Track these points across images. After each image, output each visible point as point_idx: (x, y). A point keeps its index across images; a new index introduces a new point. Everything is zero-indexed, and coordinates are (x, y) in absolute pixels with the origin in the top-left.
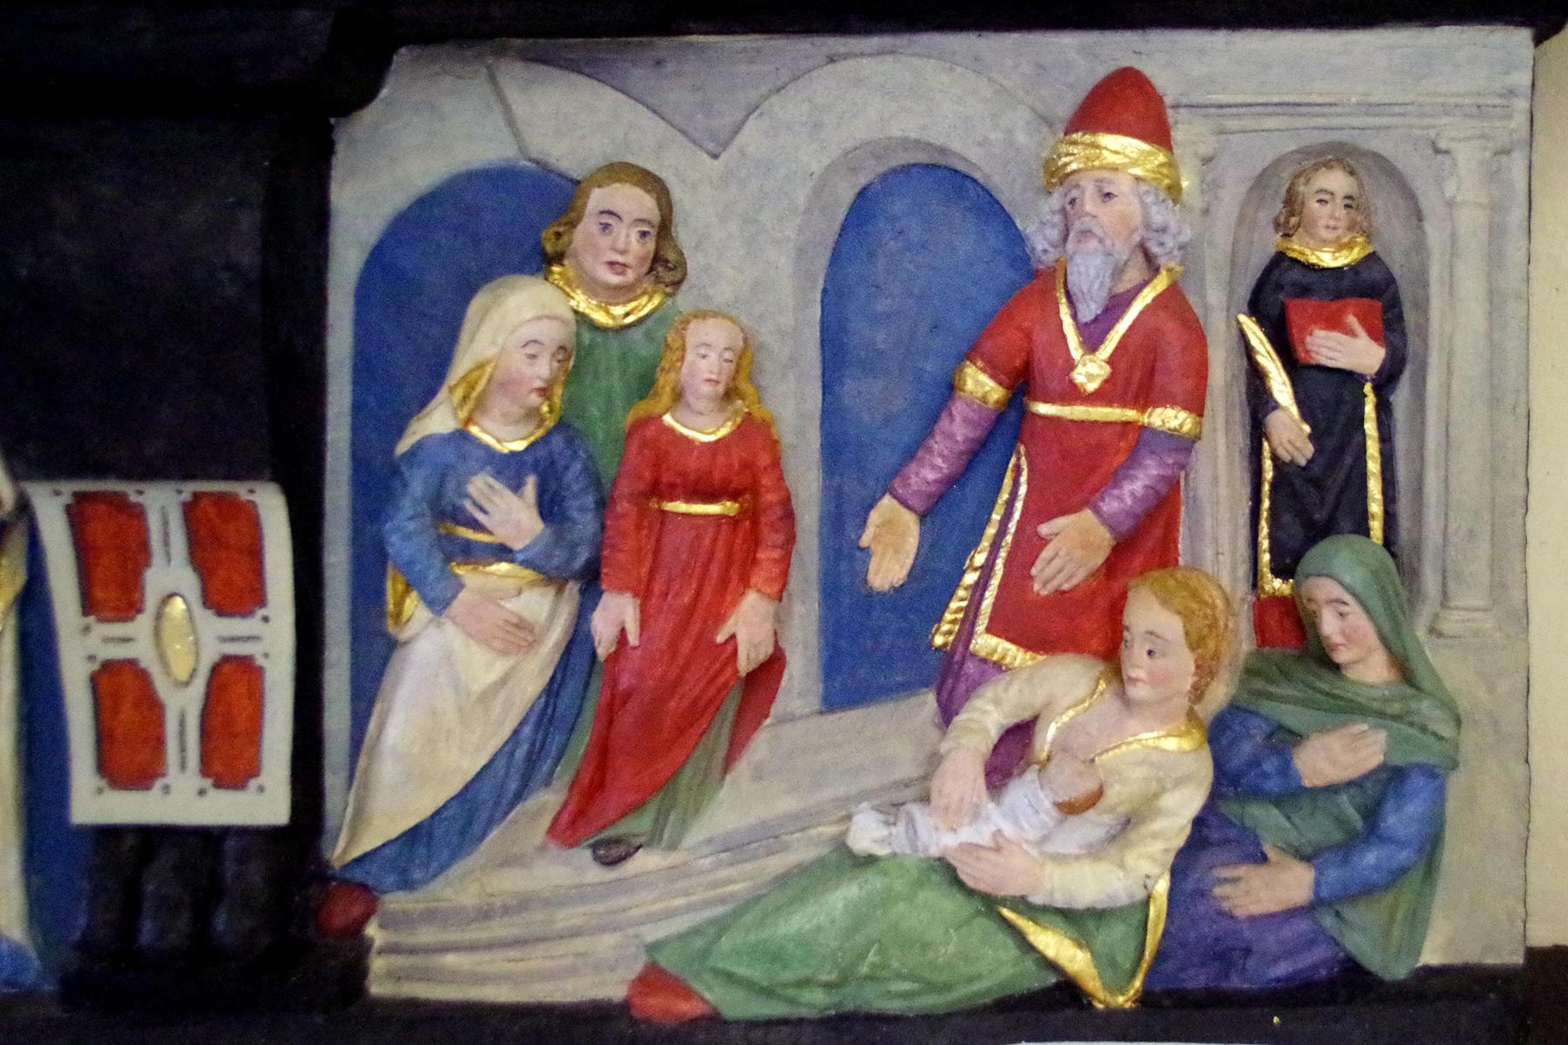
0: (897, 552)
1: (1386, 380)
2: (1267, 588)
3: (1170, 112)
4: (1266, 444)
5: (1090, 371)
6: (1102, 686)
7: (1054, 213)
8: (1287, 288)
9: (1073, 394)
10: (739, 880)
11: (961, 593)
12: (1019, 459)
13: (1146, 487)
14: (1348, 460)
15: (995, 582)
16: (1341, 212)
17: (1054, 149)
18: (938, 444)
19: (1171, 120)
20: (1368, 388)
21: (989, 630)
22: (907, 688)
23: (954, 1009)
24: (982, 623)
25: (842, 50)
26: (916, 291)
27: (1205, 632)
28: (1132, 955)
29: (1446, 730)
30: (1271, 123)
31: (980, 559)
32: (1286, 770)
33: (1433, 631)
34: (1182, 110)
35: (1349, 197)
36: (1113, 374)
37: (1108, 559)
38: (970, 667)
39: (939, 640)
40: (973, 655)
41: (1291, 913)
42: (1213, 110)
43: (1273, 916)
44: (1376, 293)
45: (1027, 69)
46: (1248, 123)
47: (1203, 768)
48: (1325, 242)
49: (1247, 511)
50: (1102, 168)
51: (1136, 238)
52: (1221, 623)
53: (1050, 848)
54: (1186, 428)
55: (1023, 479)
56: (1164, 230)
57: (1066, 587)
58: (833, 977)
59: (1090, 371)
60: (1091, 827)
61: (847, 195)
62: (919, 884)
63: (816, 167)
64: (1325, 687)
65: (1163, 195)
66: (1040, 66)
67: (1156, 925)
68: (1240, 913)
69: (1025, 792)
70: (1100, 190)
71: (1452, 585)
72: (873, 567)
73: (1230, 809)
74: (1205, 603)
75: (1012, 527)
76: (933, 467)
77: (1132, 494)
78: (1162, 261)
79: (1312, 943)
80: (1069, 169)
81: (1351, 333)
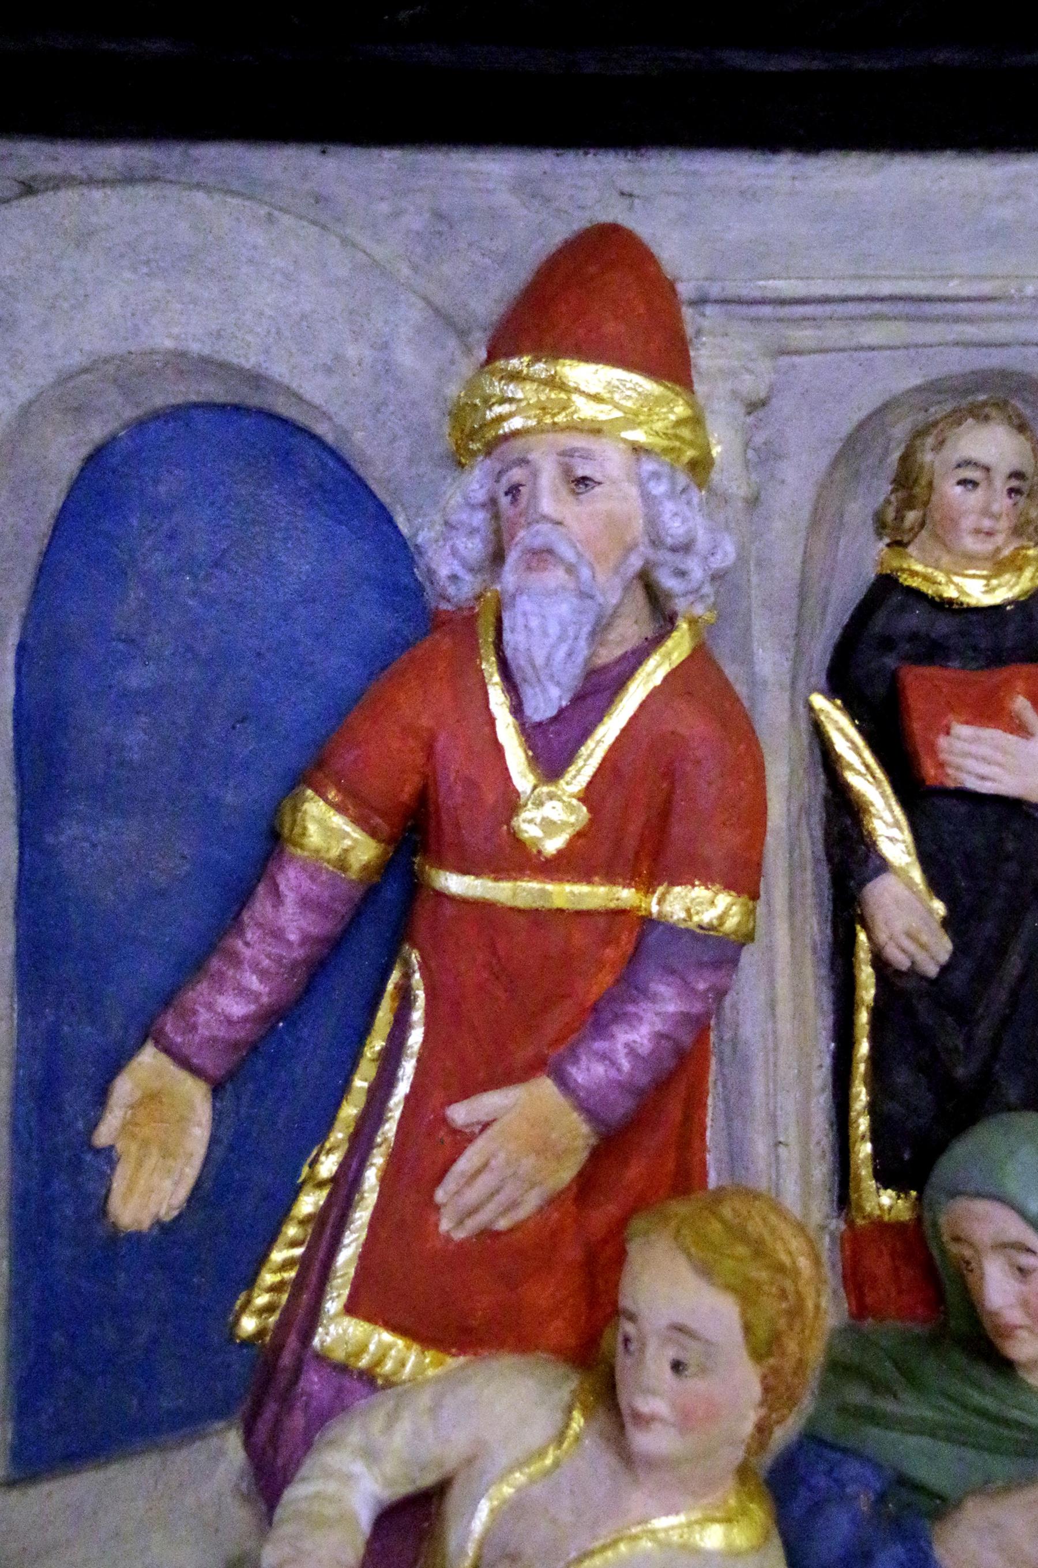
0: (167, 1153)
2: (869, 1207)
3: (687, 312)
4: (862, 936)
5: (550, 815)
6: (578, 1421)
7: (473, 507)
9: (517, 859)
11: (292, 1231)
12: (407, 976)
13: (660, 1036)
15: (362, 1216)
16: (1002, 503)
17: (472, 386)
18: (251, 945)
19: (689, 331)
21: (351, 1309)
22: (186, 1423)
26: (204, 651)
27: (782, 1323)
30: (874, 334)
31: (328, 1166)
34: (709, 310)
35: (1017, 475)
36: (592, 822)
37: (580, 1174)
38: (313, 1381)
39: (249, 1324)
40: (321, 1358)
42: (766, 310)
45: (414, 221)
46: (836, 334)
48: (971, 559)
49: (827, 1061)
50: (574, 427)
51: (636, 563)
52: (810, 1304)
54: (731, 923)
55: (417, 1015)
56: (685, 548)
57: (503, 1224)
59: (550, 815)
61: (63, 454)
64: (988, 1402)
65: (682, 479)
66: (439, 215)
70: (567, 471)
72: (119, 1185)
74: (780, 1269)
76: (242, 991)
77: (632, 1051)
78: (680, 605)
80: (507, 427)
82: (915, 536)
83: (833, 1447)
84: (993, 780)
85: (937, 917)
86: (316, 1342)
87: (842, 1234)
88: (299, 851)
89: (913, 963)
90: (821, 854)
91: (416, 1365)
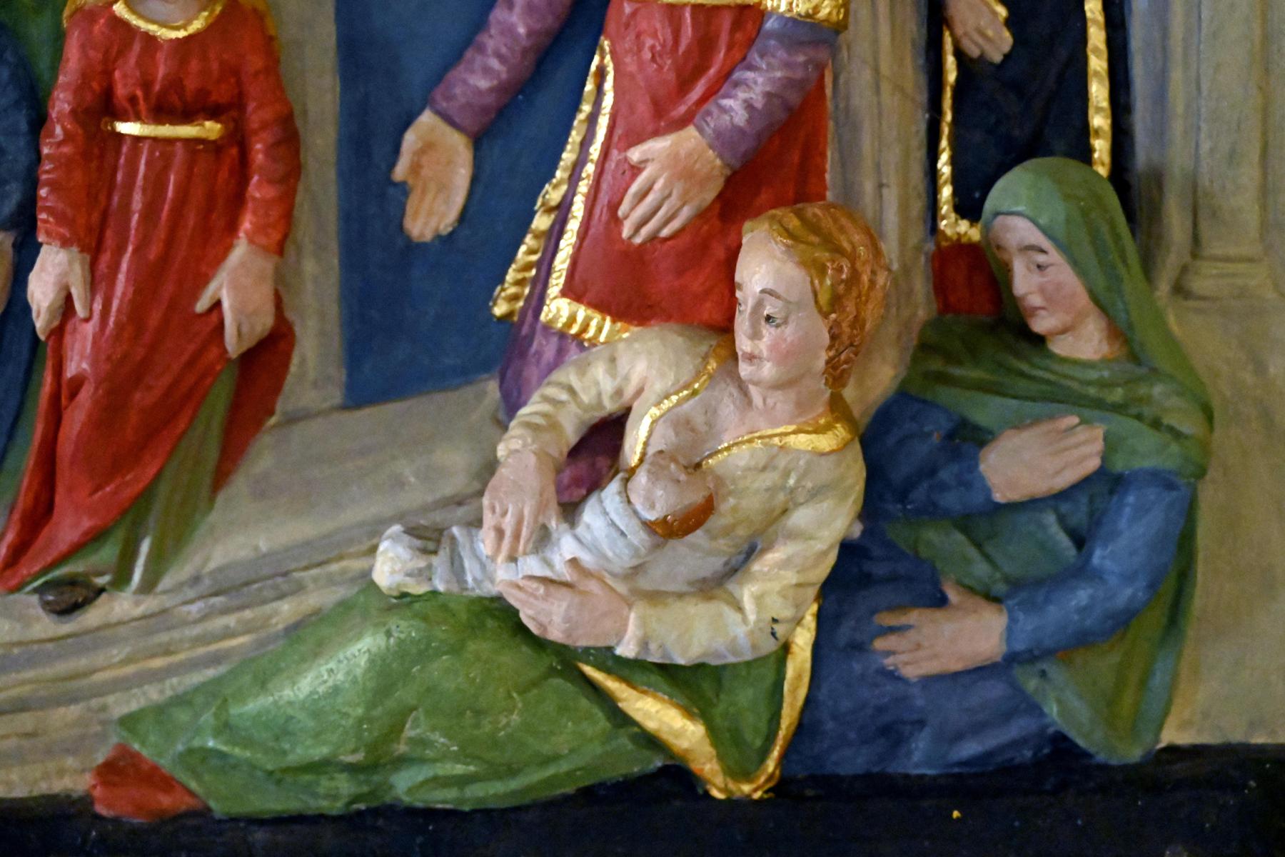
10: (235, 632)
12: (602, 58)
14: (1063, 53)
15: (573, 226)
18: (492, 40)
21: (565, 293)
22: (465, 374)
23: (527, 800)
24: (557, 282)
28: (763, 726)
29: (1189, 425)
32: (970, 479)
33: (1180, 290)
37: (720, 196)
40: (547, 328)
47: (855, 473)
52: (865, 278)
53: (644, 583)
55: (609, 85)
58: (359, 757)
60: (696, 555)
67: (794, 690)
68: (911, 672)
69: (608, 524)
71: (1204, 225)
73: (897, 533)
75: (595, 151)
76: (487, 71)
77: (749, 106)
79: (1007, 716)
83: (918, 400)
86: (543, 317)
91: (611, 332)
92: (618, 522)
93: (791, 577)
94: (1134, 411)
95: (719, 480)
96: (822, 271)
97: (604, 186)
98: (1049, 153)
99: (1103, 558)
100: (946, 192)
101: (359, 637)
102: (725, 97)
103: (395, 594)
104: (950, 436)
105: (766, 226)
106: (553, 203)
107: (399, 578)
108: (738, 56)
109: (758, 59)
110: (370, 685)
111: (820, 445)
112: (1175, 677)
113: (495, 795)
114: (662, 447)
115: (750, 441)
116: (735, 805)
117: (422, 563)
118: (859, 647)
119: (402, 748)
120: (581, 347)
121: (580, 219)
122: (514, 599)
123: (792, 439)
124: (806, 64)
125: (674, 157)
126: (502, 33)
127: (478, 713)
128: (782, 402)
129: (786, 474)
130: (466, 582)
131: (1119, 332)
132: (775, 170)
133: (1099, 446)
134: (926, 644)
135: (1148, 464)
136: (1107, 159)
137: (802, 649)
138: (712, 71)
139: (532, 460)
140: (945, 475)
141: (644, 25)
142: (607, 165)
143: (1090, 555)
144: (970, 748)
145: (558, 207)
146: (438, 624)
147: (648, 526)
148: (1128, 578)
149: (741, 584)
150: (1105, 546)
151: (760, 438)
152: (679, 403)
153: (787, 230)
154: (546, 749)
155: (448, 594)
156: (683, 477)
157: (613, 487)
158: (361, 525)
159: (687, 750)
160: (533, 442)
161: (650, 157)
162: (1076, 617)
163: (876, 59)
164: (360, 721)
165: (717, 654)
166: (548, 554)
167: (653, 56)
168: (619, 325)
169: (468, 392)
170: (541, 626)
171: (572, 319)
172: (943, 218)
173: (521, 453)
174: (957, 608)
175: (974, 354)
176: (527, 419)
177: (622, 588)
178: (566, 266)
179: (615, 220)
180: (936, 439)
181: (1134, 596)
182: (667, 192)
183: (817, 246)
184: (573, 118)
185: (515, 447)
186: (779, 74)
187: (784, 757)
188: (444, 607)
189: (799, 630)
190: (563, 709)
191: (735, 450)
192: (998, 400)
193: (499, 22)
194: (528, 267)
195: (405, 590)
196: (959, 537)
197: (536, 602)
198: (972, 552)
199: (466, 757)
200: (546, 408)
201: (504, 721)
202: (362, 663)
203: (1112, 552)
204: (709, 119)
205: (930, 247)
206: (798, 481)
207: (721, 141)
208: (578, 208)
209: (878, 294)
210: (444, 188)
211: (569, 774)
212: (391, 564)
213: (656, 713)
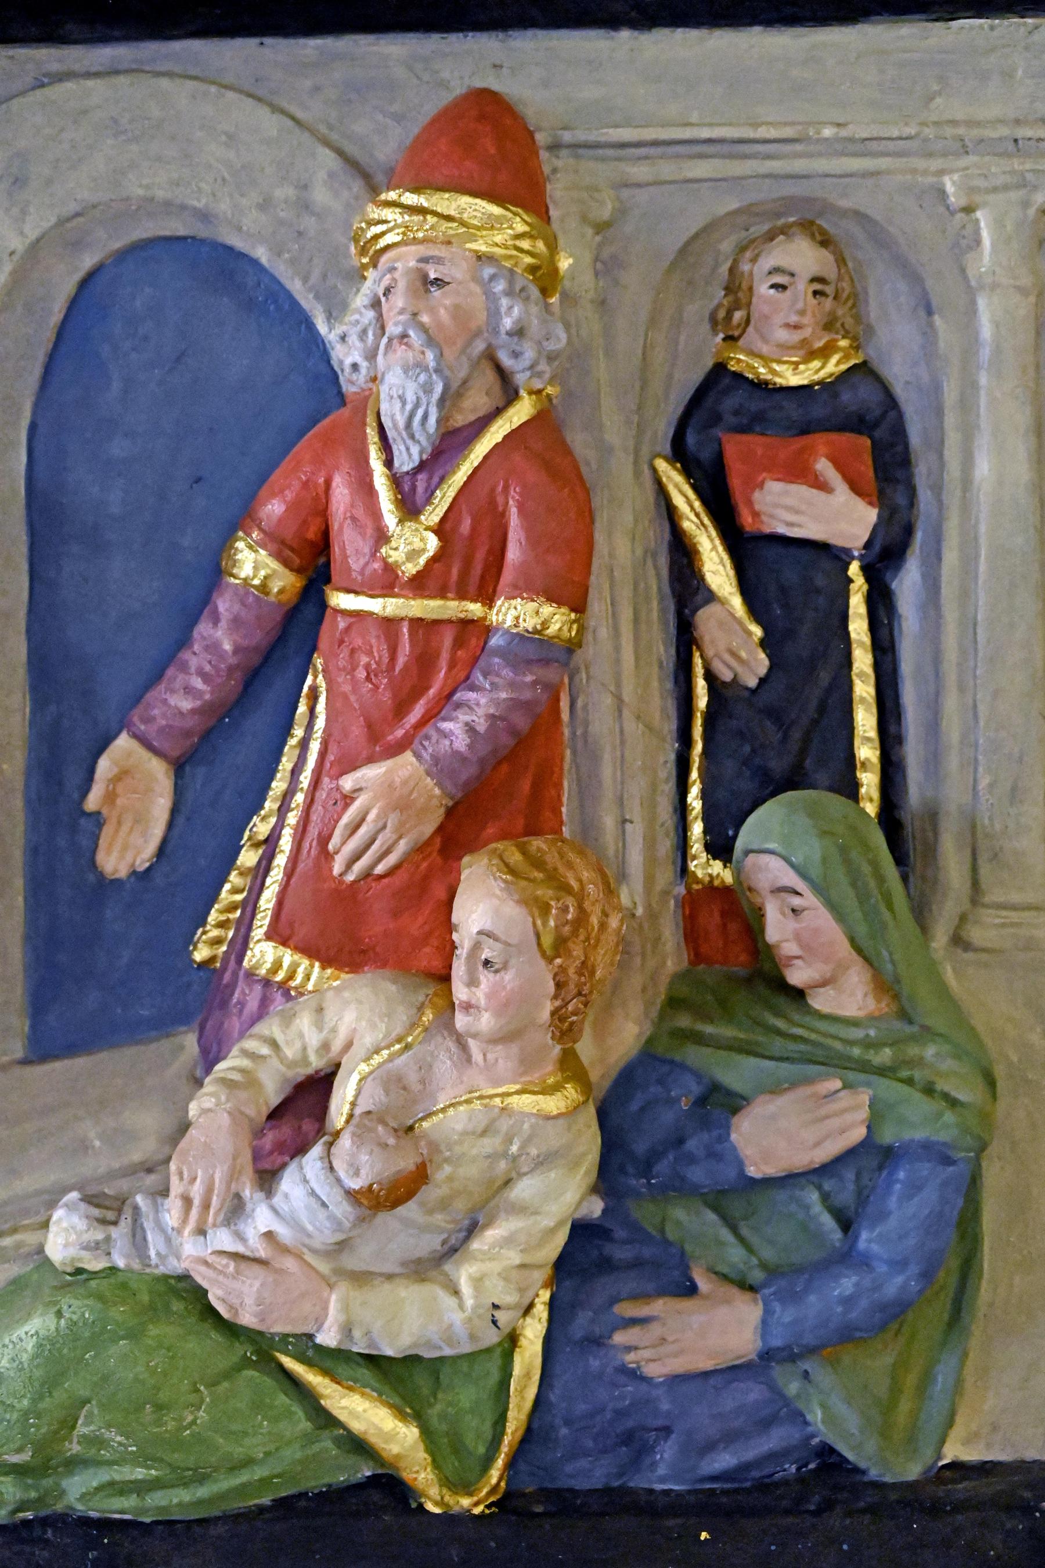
1: (884, 557)
3: (544, 155)
8: (731, 420)
12: (316, 677)
14: (824, 677)
15: (281, 861)
18: (196, 658)
19: (546, 169)
20: (854, 569)
21: (269, 936)
24: (262, 923)
25: (55, 67)
30: (701, 169)
32: (720, 1152)
33: (958, 941)
37: (440, 829)
40: (250, 975)
41: (735, 1372)
43: (706, 1375)
44: (871, 430)
46: (667, 170)
47: (589, 1143)
49: (672, 757)
52: (594, 920)
53: (351, 1262)
54: (553, 629)
55: (321, 707)
58: (25, 1457)
59: (412, 545)
60: (408, 1230)
62: (154, 1311)
63: (18, 244)
67: (521, 1392)
68: (654, 1370)
69: (308, 1194)
71: (985, 871)
73: (644, 1213)
75: (305, 779)
76: (188, 690)
77: (470, 729)
78: (520, 379)
79: (766, 1424)
80: (382, 243)
81: (822, 486)
82: (744, 331)
83: (664, 1061)
84: (800, 526)
85: (756, 640)
86: (245, 964)
87: (684, 897)
88: (232, 579)
89: (735, 676)
90: (667, 589)
92: (318, 1191)
93: (514, 1257)
94: (904, 1074)
95: (434, 1147)
96: (545, 909)
97: (314, 817)
98: (813, 786)
99: (869, 1241)
100: (697, 829)
101: (28, 1316)
102: (444, 719)
103: (69, 1270)
104: (701, 1101)
105: (486, 861)
106: (261, 837)
107: (72, 1252)
108: (462, 675)
109: (481, 678)
110: (38, 1373)
111: (548, 1105)
112: (959, 1384)
113: (180, 1504)
114: (371, 1108)
115: (468, 1102)
116: (451, 1520)
117: (100, 1236)
118: (596, 1342)
119: (75, 1448)
120: (287, 995)
121: (287, 853)
122: (202, 1277)
123: (514, 1100)
124: (535, 683)
125: (388, 785)
126: (207, 648)
127: (159, 1407)
128: (504, 1058)
129: (509, 1141)
130: (149, 1257)
131: (885, 985)
132: (503, 797)
133: (864, 1113)
134: (670, 1339)
135: (919, 1135)
136: (876, 795)
137: (532, 1342)
138: (432, 692)
139: (225, 1120)
140: (692, 1145)
141: (358, 642)
142: (317, 794)
143: (857, 1237)
144: (724, 1460)
145: (266, 841)
146: (115, 1304)
147: (352, 1195)
148: (899, 1264)
149: (458, 1264)
150: (872, 1228)
151: (481, 1098)
152: (391, 1058)
153: (507, 865)
154: (239, 1452)
155: (129, 1270)
156: (391, 1141)
157: (317, 1151)
158: (38, 1193)
159: (398, 1456)
160: (228, 1100)
161: (364, 785)
162: (839, 1309)
163: (618, 685)
164: (26, 1414)
165: (429, 1344)
166: (241, 1226)
167: (368, 674)
168: (329, 971)
169: (165, 1045)
170: (231, 1307)
171: (277, 965)
172: (694, 858)
173: (214, 1113)
174: (706, 1297)
175: (725, 1010)
176: (222, 1075)
177: (323, 1267)
178: (271, 905)
179: (326, 856)
180: (684, 1104)
181: (904, 1287)
182: (380, 824)
183: (538, 884)
184: (284, 743)
185: (208, 1106)
186: (504, 695)
187: (511, 1464)
188: (124, 1286)
189: (528, 1320)
190: (258, 1406)
191: (451, 1112)
192: (753, 1061)
193: (204, 638)
194: (232, 908)
195: (81, 1265)
196: (711, 1216)
197: (225, 1281)
198: (726, 1235)
199: (147, 1459)
200: (245, 1063)
201: (190, 1418)
202: (29, 1348)
203: (880, 1235)
204: (426, 743)
205: (681, 890)
206: (522, 1148)
207: (438, 768)
208: (286, 843)
209: (609, 939)
210: (141, 819)
211: (265, 1483)
212: (66, 1236)
213: (364, 1412)
